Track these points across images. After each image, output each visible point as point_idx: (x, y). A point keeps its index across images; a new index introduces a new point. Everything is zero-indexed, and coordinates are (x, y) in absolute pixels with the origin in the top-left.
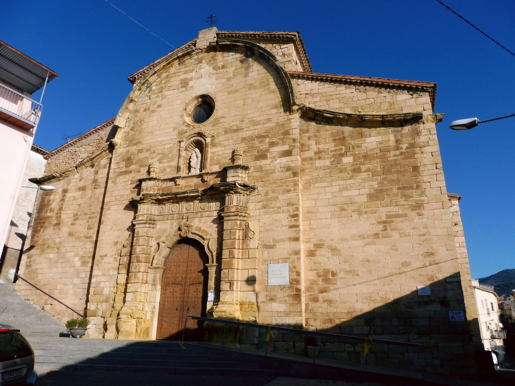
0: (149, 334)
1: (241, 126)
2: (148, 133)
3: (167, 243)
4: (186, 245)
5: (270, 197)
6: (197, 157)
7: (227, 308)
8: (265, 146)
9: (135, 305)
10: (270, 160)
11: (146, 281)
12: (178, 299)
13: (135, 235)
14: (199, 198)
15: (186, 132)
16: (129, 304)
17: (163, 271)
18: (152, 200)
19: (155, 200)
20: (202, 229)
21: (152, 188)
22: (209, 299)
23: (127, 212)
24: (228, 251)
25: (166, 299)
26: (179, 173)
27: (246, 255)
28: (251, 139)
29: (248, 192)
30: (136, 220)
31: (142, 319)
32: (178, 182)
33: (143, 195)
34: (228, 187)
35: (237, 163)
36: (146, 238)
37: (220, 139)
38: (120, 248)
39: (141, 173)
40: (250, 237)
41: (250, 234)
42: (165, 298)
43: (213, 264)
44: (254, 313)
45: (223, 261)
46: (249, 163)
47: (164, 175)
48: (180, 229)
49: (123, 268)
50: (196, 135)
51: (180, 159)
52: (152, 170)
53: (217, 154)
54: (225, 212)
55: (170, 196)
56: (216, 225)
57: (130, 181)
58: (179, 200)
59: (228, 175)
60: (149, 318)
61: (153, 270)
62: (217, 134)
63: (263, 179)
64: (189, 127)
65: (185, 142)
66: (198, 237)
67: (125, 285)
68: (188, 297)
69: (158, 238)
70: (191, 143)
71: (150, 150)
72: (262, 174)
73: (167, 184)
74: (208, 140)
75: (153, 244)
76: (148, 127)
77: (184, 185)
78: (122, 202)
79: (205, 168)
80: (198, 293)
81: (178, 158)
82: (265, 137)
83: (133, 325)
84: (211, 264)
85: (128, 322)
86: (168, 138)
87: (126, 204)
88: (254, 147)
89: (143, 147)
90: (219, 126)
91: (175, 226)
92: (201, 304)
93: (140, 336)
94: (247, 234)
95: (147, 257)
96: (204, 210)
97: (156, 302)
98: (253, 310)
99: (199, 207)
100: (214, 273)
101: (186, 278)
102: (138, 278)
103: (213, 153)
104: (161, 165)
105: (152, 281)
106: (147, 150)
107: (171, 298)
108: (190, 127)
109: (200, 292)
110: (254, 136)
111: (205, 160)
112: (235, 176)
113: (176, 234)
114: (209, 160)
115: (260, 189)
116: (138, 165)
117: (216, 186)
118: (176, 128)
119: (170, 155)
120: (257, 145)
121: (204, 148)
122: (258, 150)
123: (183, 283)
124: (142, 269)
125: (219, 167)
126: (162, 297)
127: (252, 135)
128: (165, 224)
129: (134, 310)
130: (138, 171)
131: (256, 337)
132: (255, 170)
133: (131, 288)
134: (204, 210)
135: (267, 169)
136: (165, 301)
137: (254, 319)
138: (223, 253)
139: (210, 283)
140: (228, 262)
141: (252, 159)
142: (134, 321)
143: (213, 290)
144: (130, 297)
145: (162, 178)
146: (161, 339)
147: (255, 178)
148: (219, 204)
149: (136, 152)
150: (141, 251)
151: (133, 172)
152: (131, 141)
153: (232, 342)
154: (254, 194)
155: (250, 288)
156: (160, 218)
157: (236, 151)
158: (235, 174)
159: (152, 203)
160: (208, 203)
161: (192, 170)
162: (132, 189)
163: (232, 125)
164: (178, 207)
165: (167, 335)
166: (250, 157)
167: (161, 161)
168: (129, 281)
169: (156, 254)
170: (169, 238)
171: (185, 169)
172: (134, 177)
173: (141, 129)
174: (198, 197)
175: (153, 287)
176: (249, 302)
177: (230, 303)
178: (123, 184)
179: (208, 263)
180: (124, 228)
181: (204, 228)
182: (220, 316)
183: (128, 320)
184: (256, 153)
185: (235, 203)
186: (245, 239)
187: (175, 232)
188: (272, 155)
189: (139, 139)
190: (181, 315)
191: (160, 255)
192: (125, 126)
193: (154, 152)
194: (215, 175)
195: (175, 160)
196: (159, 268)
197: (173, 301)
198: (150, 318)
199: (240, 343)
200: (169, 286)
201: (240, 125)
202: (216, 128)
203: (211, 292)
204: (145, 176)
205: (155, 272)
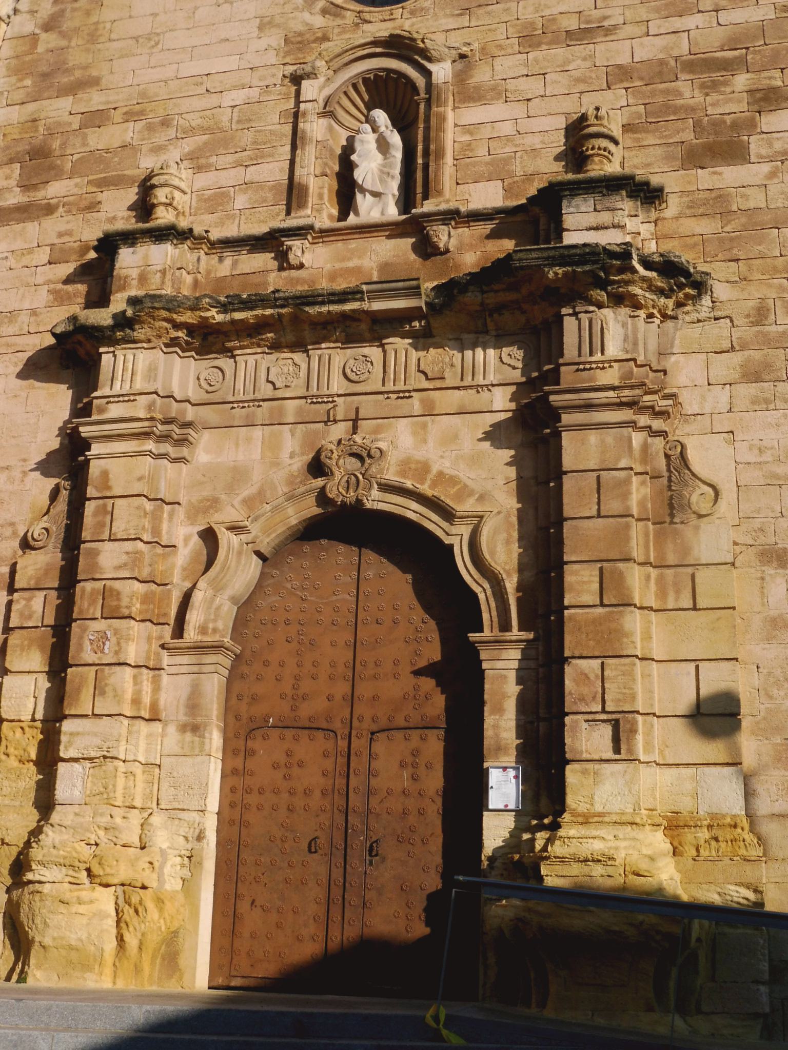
0: (182, 962)
1: (605, 18)
2: (132, 42)
3: (254, 533)
4: (341, 548)
5: (780, 329)
6: (383, 146)
7: (613, 844)
8: (731, 108)
9: (104, 820)
10: (766, 168)
11: (154, 707)
12: (316, 800)
13: (91, 491)
14: (416, 324)
15: (325, 38)
16: (76, 814)
17: (228, 663)
18: (177, 326)
19: (190, 329)
20: (434, 471)
21: (169, 276)
22: (495, 800)
23: (34, 388)
24: (594, 571)
25: (253, 799)
26: (302, 213)
27: (678, 592)
28: (660, 73)
29: (670, 303)
30: (94, 417)
31: (144, 887)
32: (299, 253)
33: (134, 301)
34: (587, 268)
35: (599, 168)
36: (149, 506)
37: (498, 68)
38: (8, 553)
39: (102, 216)
40: (695, 507)
41: (698, 497)
42: (248, 791)
43: (508, 636)
44: (748, 867)
45: (570, 618)
46: (650, 176)
47: (221, 223)
48: (317, 467)
49: (29, 647)
50: (379, 50)
51: (299, 152)
52: (163, 200)
53: (486, 132)
54: (563, 386)
55: (268, 312)
56: (507, 454)
57: (48, 249)
58: (307, 334)
59: (569, 220)
60: (173, 884)
61: (186, 659)
62: (483, 50)
63: (735, 251)
64: (336, 15)
65: (322, 79)
66: (415, 506)
67: (39, 724)
68: (370, 792)
69: (205, 511)
70: (355, 86)
71: (142, 113)
72: (727, 229)
73: (235, 264)
74: (442, 72)
75: (181, 538)
76: (130, 17)
77: (328, 267)
78: (8, 345)
79: (432, 192)
80: (422, 770)
81: (288, 148)
82: (727, 66)
83: (102, 915)
84: (496, 632)
85: (80, 902)
86: (232, 63)
87: (30, 354)
88: (676, 110)
89: (108, 102)
90: (489, 13)
91: (292, 456)
92: (438, 822)
93: (138, 969)
94: (681, 496)
95: (153, 593)
96: (438, 384)
97: (209, 809)
98: (743, 852)
99: (413, 367)
100: (512, 676)
101: (352, 699)
102: (115, 690)
103: (468, 129)
104: (204, 180)
105: (182, 710)
106: (130, 116)
107: (276, 792)
108: (344, 17)
109: (429, 766)
110: (673, 63)
111: (432, 158)
112: (606, 228)
113: (302, 489)
114: (449, 159)
115: (721, 291)
116: (86, 179)
117: (525, 263)
118: (270, 23)
119: (247, 138)
120: (691, 101)
121: (422, 106)
122: (697, 124)
123: (337, 725)
124: (132, 653)
125: (501, 192)
126: (233, 790)
127: (661, 56)
128: (237, 445)
129: (102, 845)
130: (84, 204)
131: (763, 983)
132: (689, 207)
133: (80, 742)
134: (438, 384)
135: (751, 204)
136: (246, 807)
137: (751, 896)
138: (569, 579)
139: (496, 727)
140: (596, 621)
141: (668, 158)
142: (105, 899)
143: (510, 759)
144: (79, 783)
145: (214, 235)
146: (234, 983)
147: (695, 245)
148: (520, 354)
149: (76, 122)
150: (125, 565)
151: (61, 209)
152: (45, 76)
153: (650, 1009)
154: (694, 316)
155: (715, 750)
156: (206, 413)
157: (592, 120)
158: (605, 217)
159: (174, 343)
160: (462, 350)
161: (363, 202)
162: (60, 286)
163: (555, 11)
164: (304, 366)
165: (267, 969)
166: (659, 151)
167: (202, 161)
168: (70, 705)
169: (202, 584)
170: (268, 507)
171: (326, 197)
172: (69, 233)
173: (98, 23)
174: (410, 321)
175: (188, 736)
176: (713, 816)
177: (624, 819)
178: (12, 262)
179: (482, 631)
180: (25, 460)
181: (442, 463)
182: (581, 879)
183: (76, 894)
184: (688, 136)
185: (613, 349)
186: (668, 519)
187: (291, 480)
188: (770, 144)
189: (85, 68)
190: (337, 874)
191: (218, 588)
192: (16, 11)
193: (166, 123)
194: (487, 228)
195: (270, 156)
196: (217, 648)
197: (290, 809)
198: (178, 885)
199: (682, 1009)
200: (265, 738)
201: (596, 14)
202: (472, 24)
203: (505, 769)
204: (125, 221)
205: (195, 669)
